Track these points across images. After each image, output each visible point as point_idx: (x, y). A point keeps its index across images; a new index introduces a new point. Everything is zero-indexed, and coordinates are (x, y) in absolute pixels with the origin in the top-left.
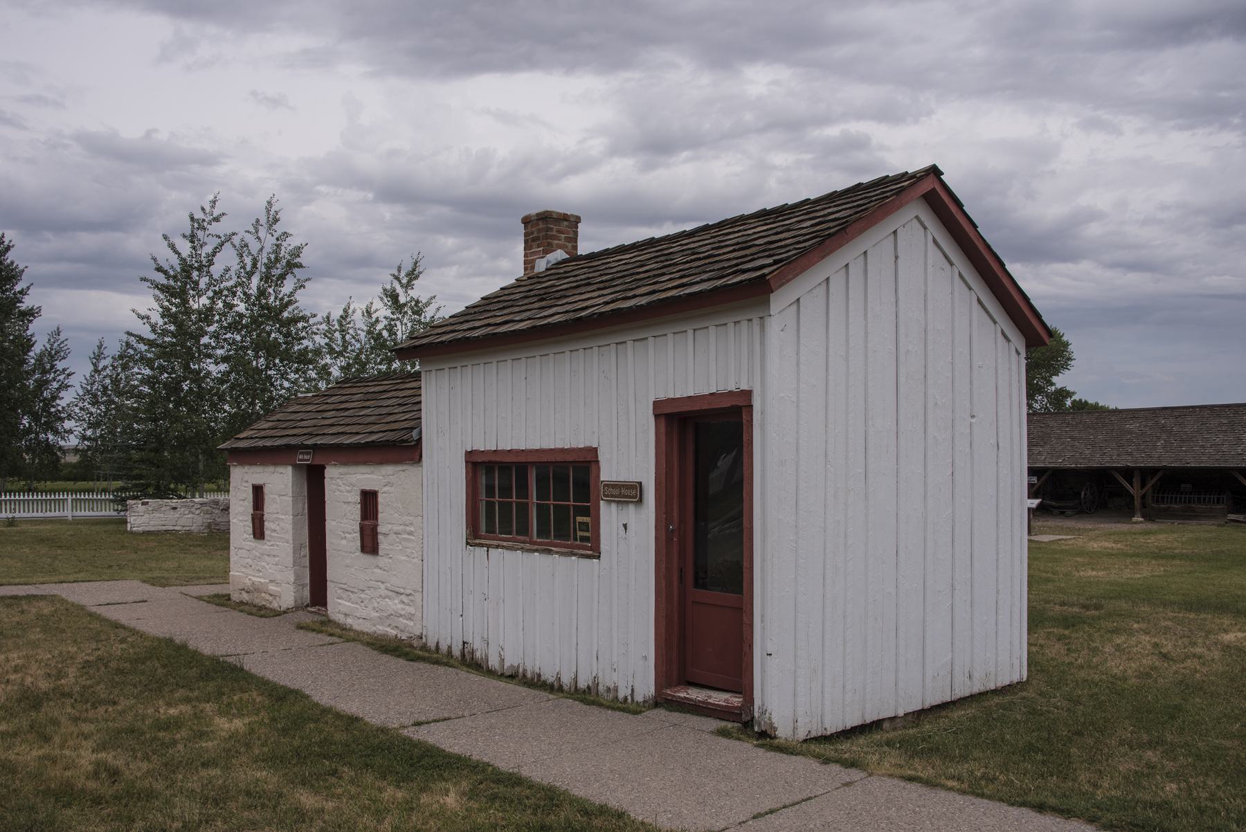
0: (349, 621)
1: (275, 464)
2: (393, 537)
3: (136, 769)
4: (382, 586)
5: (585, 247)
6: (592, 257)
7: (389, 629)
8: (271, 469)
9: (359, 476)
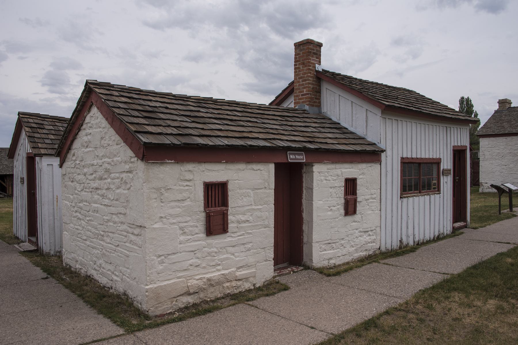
0: (332, 262)
1: (249, 162)
2: (364, 202)
3: (451, 331)
4: (357, 231)
5: (512, 106)
6: (514, 107)
7: (361, 253)
8: (242, 166)
9: (344, 170)
